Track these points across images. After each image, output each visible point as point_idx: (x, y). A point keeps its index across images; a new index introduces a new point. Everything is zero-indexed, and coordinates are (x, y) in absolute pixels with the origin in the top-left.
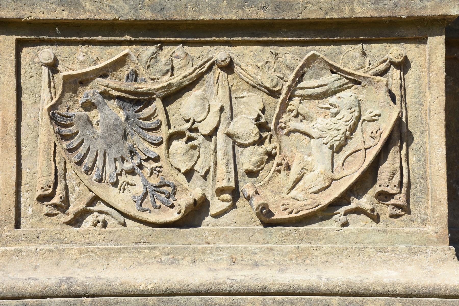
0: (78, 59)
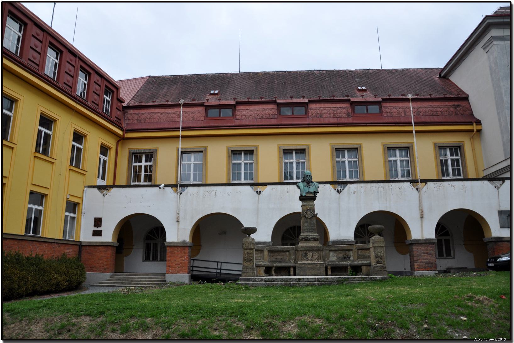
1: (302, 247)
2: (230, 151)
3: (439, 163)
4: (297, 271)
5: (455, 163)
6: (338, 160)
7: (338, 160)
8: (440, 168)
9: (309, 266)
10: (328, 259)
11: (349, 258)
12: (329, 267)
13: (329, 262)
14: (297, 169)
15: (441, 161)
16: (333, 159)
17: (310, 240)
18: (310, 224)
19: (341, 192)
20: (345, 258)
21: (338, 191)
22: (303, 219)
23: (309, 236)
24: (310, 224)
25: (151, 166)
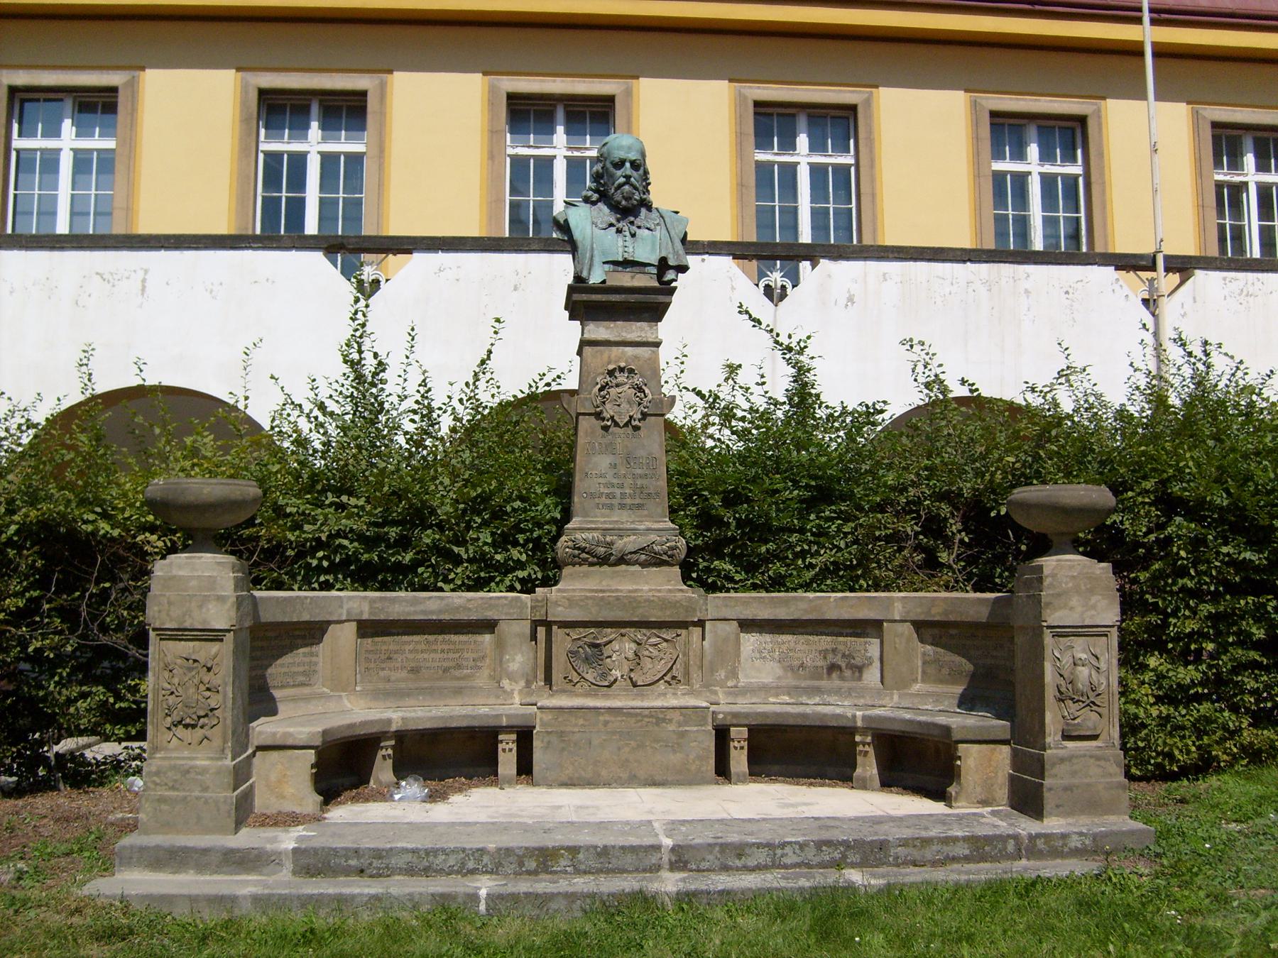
0: (575, 634)
1: (571, 602)
2: (254, 96)
3: (751, 180)
4: (538, 755)
5: (1063, 193)
6: (999, 166)
7: (999, 166)
8: (989, 212)
9: (617, 723)
10: (733, 674)
11: (859, 670)
12: (739, 734)
13: (738, 691)
14: (323, 188)
15: (999, 177)
16: (740, 153)
17: (622, 560)
18: (629, 459)
19: (783, 295)
20: (833, 668)
21: (768, 291)
22: (586, 424)
23: (622, 533)
24: (629, 459)
25: (355, 160)
